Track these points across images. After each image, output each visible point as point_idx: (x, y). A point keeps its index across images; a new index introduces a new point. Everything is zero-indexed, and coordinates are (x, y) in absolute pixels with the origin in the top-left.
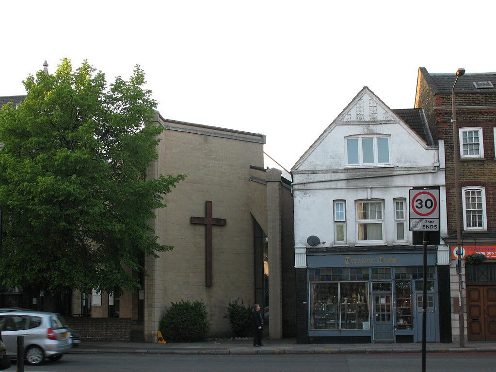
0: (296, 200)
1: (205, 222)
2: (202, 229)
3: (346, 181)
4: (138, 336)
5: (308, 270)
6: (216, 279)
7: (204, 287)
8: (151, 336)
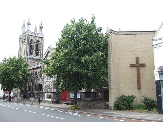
0: (154, 52)
1: (136, 65)
2: (135, 69)
3: (134, 35)
4: (107, 107)
5: (161, 81)
6: (142, 86)
7: (137, 89)
8: (111, 107)
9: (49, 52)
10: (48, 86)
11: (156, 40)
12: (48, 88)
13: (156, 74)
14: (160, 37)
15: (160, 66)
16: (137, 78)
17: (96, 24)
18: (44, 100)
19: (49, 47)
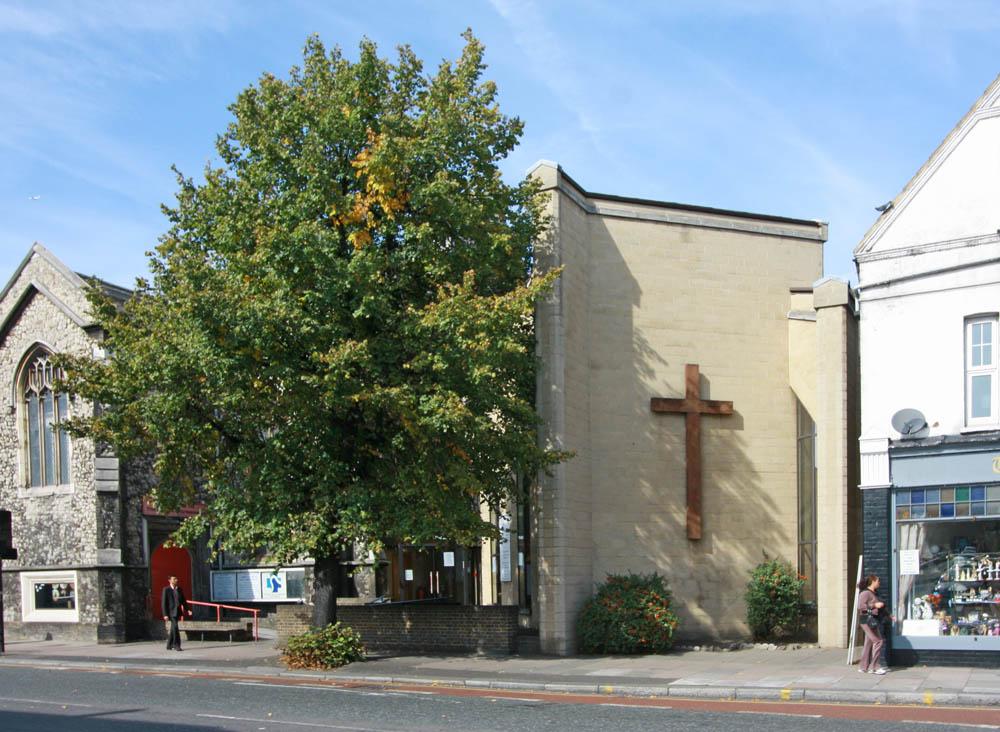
1: (683, 409)
8: (553, 642)
9: (31, 293)
10: (40, 527)
11: (884, 256)
12: (41, 538)
13: (869, 454)
14: (911, 242)
15: (895, 412)
16: (683, 482)
17: (150, 266)
18: (18, 619)
19: (28, 260)
